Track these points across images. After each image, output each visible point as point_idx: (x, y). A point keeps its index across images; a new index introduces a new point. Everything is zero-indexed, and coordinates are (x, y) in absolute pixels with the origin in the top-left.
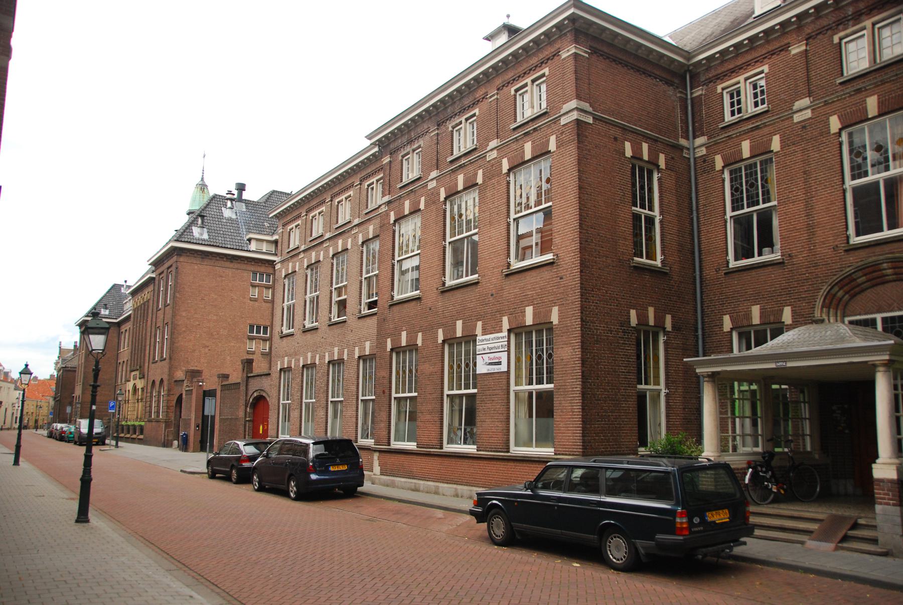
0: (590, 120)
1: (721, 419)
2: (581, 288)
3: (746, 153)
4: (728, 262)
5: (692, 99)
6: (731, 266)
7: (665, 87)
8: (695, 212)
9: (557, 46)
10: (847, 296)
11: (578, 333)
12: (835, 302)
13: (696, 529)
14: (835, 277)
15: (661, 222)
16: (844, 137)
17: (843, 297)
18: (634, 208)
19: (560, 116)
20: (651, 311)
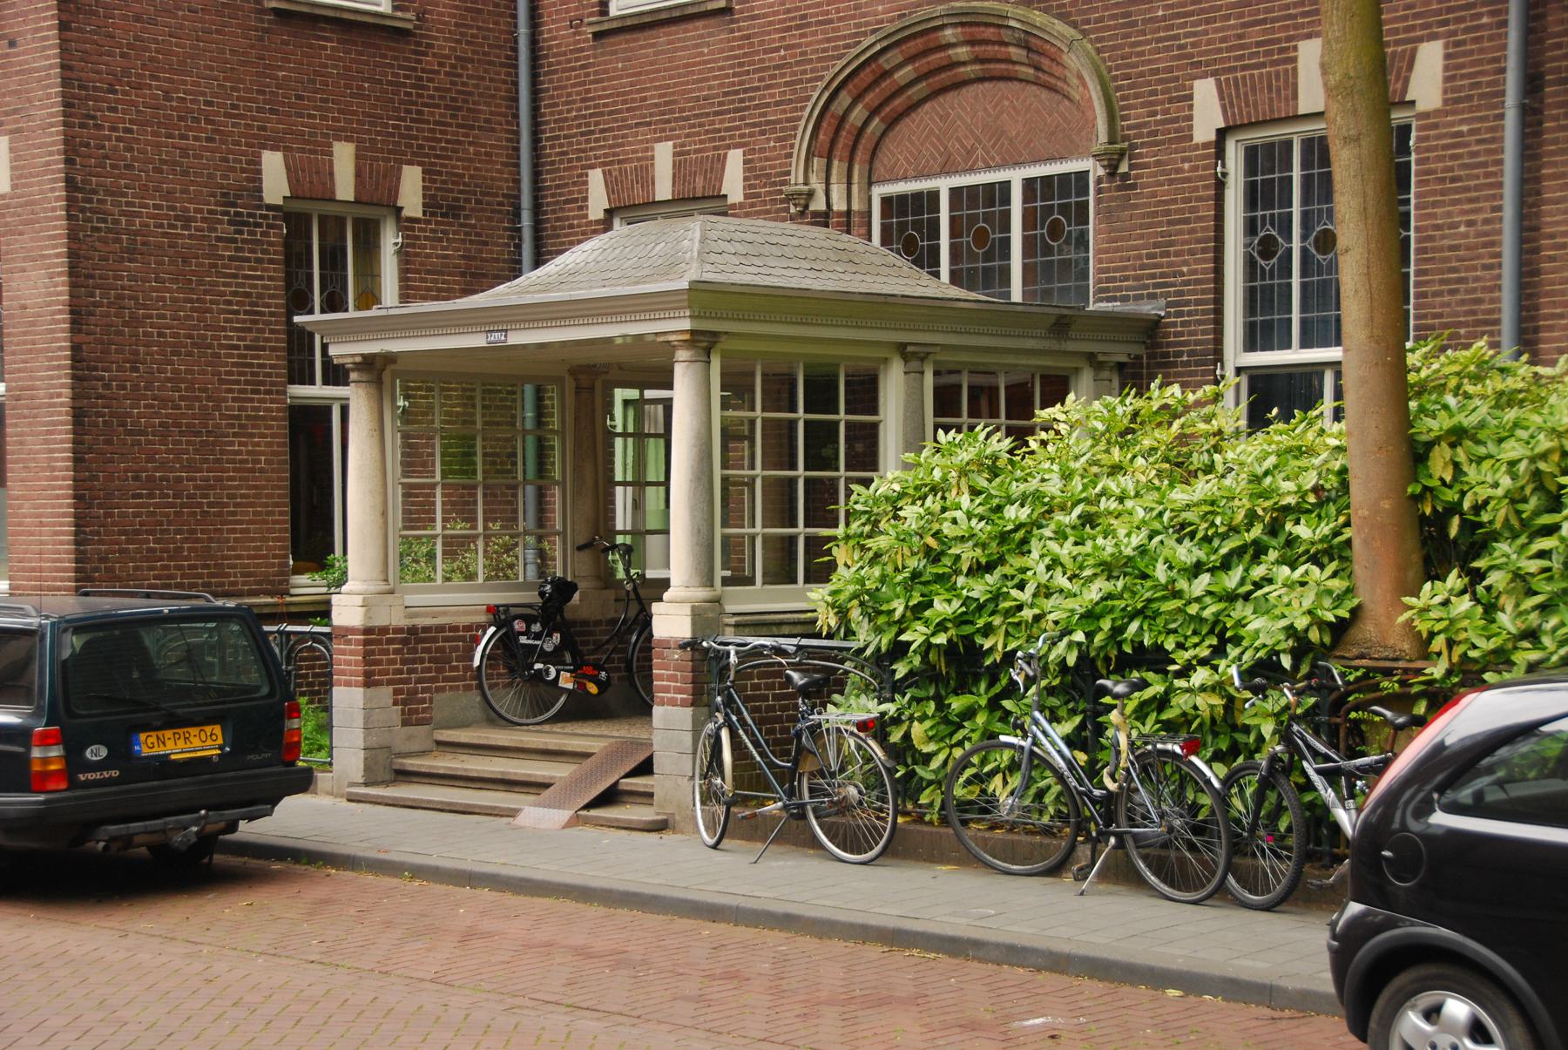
1: (409, 492)
2: (66, 82)
11: (59, 227)
12: (844, 139)
13: (91, 776)
14: (840, 63)
17: (866, 123)
20: (344, 157)
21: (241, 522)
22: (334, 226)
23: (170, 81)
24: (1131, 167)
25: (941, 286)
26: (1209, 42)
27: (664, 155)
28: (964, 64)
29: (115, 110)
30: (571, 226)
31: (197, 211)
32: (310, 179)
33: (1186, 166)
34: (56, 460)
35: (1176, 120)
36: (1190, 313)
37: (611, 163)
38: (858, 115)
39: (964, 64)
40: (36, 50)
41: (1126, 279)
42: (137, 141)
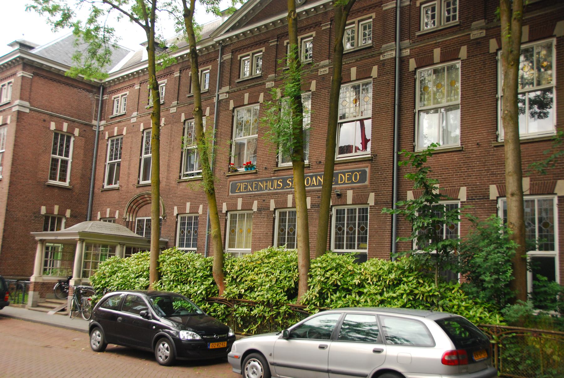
0: (27, 111)
4: (103, 186)
7: (87, 93)
12: (132, 210)
15: (72, 163)
20: (56, 208)
22: (53, 218)
25: (135, 235)
27: (108, 210)
32: (50, 210)
38: (134, 207)
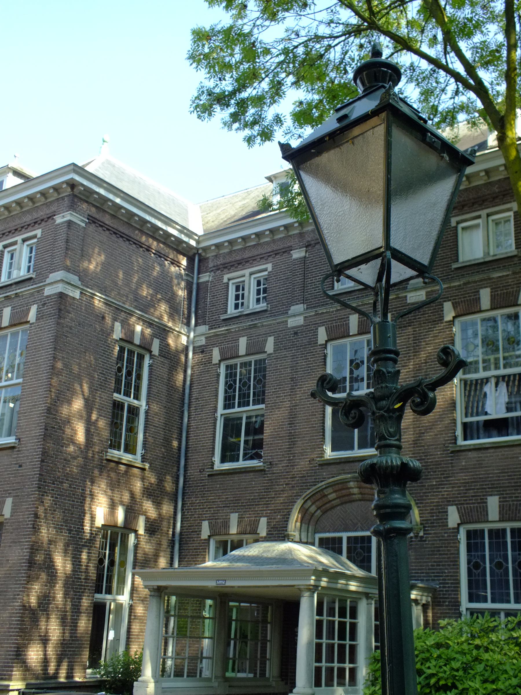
3: (242, 351)
4: (213, 464)
5: (198, 284)
6: (216, 467)
8: (186, 406)
9: (53, 208)
10: (319, 511)
16: (329, 351)
18: (115, 395)
19: (44, 285)
21: (73, 647)
23: (72, 481)
24: (424, 534)
26: (453, 494)
28: (355, 494)
29: (53, 490)
30: (194, 541)
31: (74, 527)
33: (446, 535)
34: (13, 621)
35: (441, 519)
36: (449, 587)
37: (212, 519)
39: (355, 494)
40: (30, 468)
41: (423, 573)
42: (59, 501)
